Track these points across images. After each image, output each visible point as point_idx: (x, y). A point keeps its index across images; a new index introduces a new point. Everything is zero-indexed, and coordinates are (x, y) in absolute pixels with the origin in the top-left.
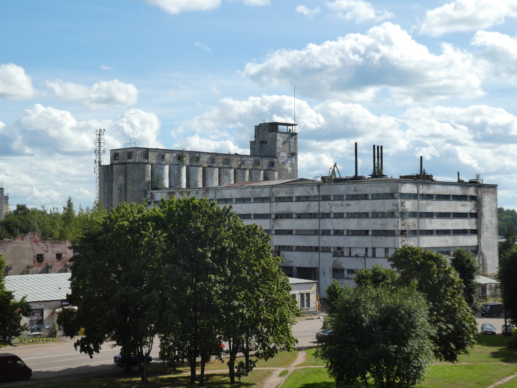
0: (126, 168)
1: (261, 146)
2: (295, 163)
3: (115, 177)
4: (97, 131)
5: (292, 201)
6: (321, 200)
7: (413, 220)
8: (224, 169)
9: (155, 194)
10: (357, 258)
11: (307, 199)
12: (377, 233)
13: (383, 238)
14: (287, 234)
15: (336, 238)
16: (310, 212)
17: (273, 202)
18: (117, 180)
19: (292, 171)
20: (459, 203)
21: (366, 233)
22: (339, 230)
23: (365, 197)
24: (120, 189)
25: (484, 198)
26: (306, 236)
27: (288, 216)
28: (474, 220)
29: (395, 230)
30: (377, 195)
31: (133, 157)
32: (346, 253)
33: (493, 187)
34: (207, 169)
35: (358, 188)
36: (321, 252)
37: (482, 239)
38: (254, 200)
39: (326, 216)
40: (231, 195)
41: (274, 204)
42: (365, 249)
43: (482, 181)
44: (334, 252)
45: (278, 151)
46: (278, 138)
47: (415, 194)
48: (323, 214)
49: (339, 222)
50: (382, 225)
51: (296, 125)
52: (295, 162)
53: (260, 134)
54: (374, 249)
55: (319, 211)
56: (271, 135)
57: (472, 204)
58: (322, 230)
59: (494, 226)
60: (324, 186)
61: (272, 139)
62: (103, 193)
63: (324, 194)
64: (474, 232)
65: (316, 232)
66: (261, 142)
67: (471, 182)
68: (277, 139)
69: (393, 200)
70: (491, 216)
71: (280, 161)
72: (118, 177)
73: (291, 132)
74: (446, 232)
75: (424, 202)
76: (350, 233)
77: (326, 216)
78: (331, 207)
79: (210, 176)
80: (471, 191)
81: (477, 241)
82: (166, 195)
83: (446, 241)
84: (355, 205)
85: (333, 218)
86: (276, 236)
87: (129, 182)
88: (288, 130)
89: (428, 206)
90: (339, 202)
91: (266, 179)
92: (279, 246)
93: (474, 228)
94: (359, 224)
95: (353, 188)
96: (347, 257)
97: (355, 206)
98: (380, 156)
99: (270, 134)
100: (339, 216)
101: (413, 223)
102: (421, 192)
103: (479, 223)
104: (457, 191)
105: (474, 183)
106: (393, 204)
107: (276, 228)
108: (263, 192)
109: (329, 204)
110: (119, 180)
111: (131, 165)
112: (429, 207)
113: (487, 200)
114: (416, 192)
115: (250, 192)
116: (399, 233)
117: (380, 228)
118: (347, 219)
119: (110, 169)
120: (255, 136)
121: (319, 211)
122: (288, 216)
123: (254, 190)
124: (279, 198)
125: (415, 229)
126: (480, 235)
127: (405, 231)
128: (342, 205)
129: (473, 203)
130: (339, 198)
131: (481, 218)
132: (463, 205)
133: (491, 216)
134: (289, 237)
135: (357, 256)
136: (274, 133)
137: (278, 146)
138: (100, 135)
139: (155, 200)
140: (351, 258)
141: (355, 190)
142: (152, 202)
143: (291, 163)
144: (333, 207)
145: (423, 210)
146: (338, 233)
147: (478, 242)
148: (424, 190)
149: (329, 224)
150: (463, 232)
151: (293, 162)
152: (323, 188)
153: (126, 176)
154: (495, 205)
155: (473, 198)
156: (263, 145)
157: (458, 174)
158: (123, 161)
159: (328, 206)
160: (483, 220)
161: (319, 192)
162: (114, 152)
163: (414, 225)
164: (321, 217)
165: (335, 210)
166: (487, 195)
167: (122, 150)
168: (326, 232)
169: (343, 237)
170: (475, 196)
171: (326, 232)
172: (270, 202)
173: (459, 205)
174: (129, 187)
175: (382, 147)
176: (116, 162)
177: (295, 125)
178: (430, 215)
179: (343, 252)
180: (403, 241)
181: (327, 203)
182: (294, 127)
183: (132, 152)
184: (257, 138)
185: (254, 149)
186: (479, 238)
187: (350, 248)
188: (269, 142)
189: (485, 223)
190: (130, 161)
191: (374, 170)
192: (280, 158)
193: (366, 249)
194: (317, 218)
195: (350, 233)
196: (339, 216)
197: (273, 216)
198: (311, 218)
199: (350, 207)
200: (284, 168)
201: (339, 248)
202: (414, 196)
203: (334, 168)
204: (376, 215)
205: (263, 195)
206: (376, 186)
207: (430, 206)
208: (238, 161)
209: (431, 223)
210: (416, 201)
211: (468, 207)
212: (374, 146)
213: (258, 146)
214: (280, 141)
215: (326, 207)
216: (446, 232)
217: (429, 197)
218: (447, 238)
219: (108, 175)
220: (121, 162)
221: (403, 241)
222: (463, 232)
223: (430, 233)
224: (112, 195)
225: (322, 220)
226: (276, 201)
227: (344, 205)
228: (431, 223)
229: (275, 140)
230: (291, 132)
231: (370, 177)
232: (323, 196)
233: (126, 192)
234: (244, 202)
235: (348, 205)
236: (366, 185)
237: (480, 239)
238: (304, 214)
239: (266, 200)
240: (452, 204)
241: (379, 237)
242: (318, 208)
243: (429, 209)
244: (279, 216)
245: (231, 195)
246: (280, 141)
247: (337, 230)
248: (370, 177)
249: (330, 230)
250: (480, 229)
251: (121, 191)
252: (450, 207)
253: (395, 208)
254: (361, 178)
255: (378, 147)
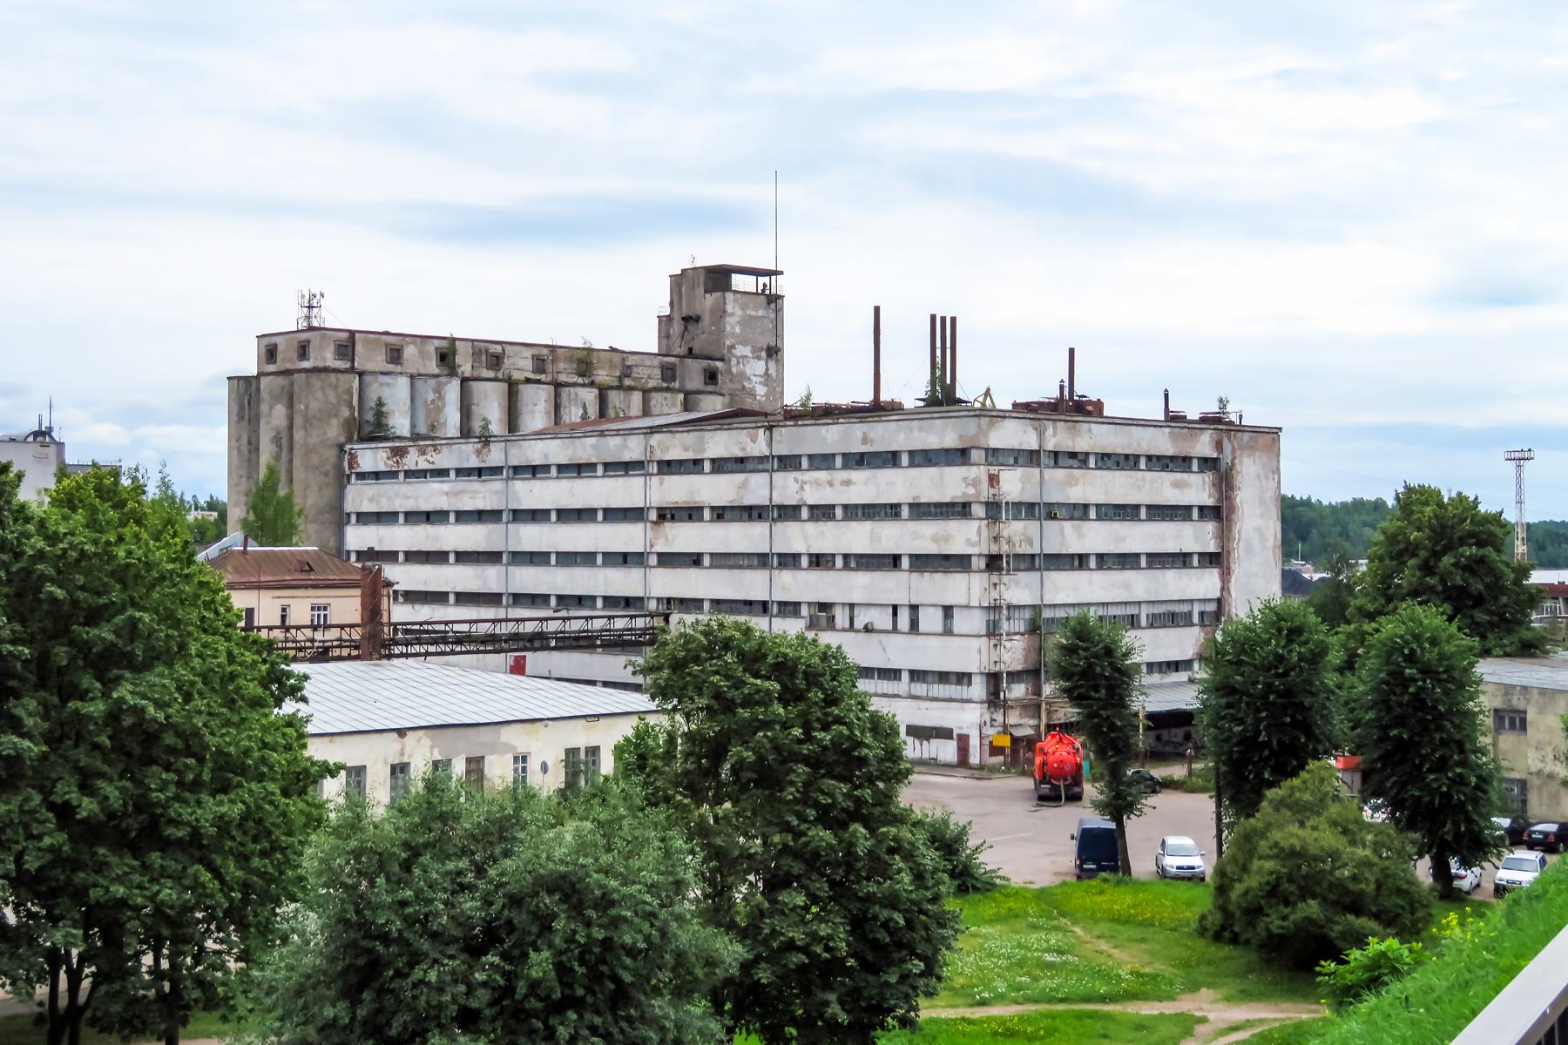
0: (292, 385)
1: (686, 329)
2: (778, 375)
3: (264, 408)
4: (303, 296)
5: (701, 472)
6: (776, 467)
7: (1025, 527)
8: (572, 389)
9: (359, 452)
10: (868, 635)
11: (739, 466)
12: (922, 563)
13: (938, 576)
14: (688, 566)
15: (815, 576)
16: (747, 502)
17: (652, 474)
18: (270, 416)
19: (767, 395)
20: (1167, 478)
21: (894, 561)
22: (823, 555)
23: (891, 459)
24: (277, 440)
25: (1241, 464)
26: (736, 572)
27: (691, 513)
28: (1210, 527)
29: (970, 556)
30: (925, 452)
31: (312, 355)
32: (841, 618)
33: (1268, 437)
34: (521, 387)
35: (872, 435)
36: (776, 616)
37: (1233, 580)
38: (605, 471)
39: (788, 513)
40: (546, 456)
41: (655, 480)
42: (890, 610)
43: (1241, 417)
44: (811, 616)
45: (728, 343)
46: (729, 308)
47: (1032, 452)
48: (780, 507)
49: (823, 533)
50: (935, 539)
51: (781, 273)
52: (777, 371)
53: (684, 298)
54: (914, 608)
55: (771, 499)
56: (711, 299)
57: (1204, 482)
58: (780, 555)
59: (1270, 543)
60: (783, 429)
61: (713, 311)
62: (235, 452)
63: (785, 453)
64: (1215, 559)
65: (762, 560)
66: (687, 319)
67: (1204, 420)
68: (725, 311)
69: (964, 468)
70: (1262, 515)
71: (734, 370)
72: (271, 408)
73: (767, 292)
74: (1126, 561)
75: (1060, 474)
76: (853, 564)
77: (788, 513)
78: (802, 488)
79: (530, 407)
80: (1203, 445)
81: (1219, 585)
82: (385, 455)
83: (1127, 586)
84: (867, 482)
85: (809, 520)
86: (661, 570)
87: (298, 421)
88: (761, 287)
89: (1071, 485)
90: (822, 475)
91: (646, 412)
92: (669, 600)
93: (1212, 547)
94: (874, 538)
95: (859, 434)
96: (844, 630)
97: (866, 486)
98: (948, 344)
99: (708, 295)
100: (822, 513)
101: (1023, 534)
102: (1050, 446)
103: (1224, 535)
104: (1162, 443)
105: (1214, 421)
106: (965, 479)
107: (661, 547)
108: (627, 447)
109: (796, 480)
110: (273, 417)
111: (303, 375)
112: (1074, 489)
113: (1248, 471)
114: (1035, 447)
115: (594, 447)
116: (983, 565)
117: (932, 549)
118: (842, 523)
119: (254, 387)
120: (672, 304)
121: (771, 499)
122: (691, 513)
123: (603, 440)
124: (669, 463)
125: (1029, 551)
126: (1228, 568)
127: (999, 557)
128: (831, 484)
129: (1208, 477)
130: (822, 461)
131: (1229, 520)
132: (1176, 485)
133: (1262, 515)
134: (693, 572)
135: (868, 629)
136: (717, 295)
137: (728, 328)
138: (310, 307)
139: (358, 470)
140: (853, 634)
141: (865, 440)
142: (353, 476)
143: (766, 373)
144: (807, 487)
145: (1054, 497)
146: (820, 561)
147: (1222, 589)
148: (1058, 437)
149: (798, 537)
150: (1181, 560)
151: (772, 371)
152: (781, 435)
153: (290, 405)
154: (1273, 484)
155: (1208, 464)
156: (690, 327)
157: (1166, 396)
158: (289, 366)
159: (795, 487)
160: (1236, 528)
161: (770, 444)
162: (266, 341)
163: (1030, 542)
164: (775, 515)
165: (813, 497)
166: (1249, 456)
167: (286, 336)
168: (789, 561)
169: (832, 573)
170: (1215, 460)
171: (789, 561)
172: (645, 475)
173: (1167, 484)
174: (298, 435)
175: (953, 320)
176: (271, 368)
177: (776, 273)
178: (1080, 512)
179: (834, 617)
180: (995, 585)
181: (791, 476)
182: (773, 278)
183: (309, 342)
184: (676, 308)
185: (668, 337)
186: (1225, 576)
187: (852, 606)
188: (706, 320)
189: (1243, 534)
190: (306, 365)
191: (933, 383)
192: (734, 361)
193: (895, 608)
194: (766, 520)
195: (853, 564)
196: (822, 513)
197: (653, 516)
198: (750, 519)
199: (852, 488)
200: (744, 387)
201: (824, 607)
202: (1031, 458)
203: (985, 399)
204: (922, 511)
205: (627, 456)
206: (920, 429)
207: (1076, 484)
208: (615, 367)
209: (1081, 536)
210: (1036, 471)
211: (1197, 490)
212: (933, 317)
213: (677, 327)
214: (733, 314)
215: (788, 488)
216: (1126, 561)
217: (1079, 459)
218: (1129, 575)
219: (249, 403)
220: (283, 369)
221: (995, 585)
222: (1181, 560)
223: (1079, 561)
224: (748, 458)
225: (779, 525)
226: (660, 473)
227: (837, 484)
228: (1081, 536)
229: (720, 313)
230: (767, 292)
231: (922, 404)
232: (781, 458)
233: (291, 449)
234: (579, 476)
235: (848, 483)
236: (893, 424)
237: (1229, 581)
238: (733, 508)
239: (634, 469)
240: (1144, 479)
241: (927, 575)
242: (767, 492)
243: (1076, 495)
244: (667, 514)
245: (546, 456)
246: (733, 314)
247: (818, 556)
248: (922, 404)
249: (799, 555)
250: (1228, 552)
251: (280, 447)
252: (1139, 489)
253: (971, 491)
254: (894, 408)
255: (943, 319)
